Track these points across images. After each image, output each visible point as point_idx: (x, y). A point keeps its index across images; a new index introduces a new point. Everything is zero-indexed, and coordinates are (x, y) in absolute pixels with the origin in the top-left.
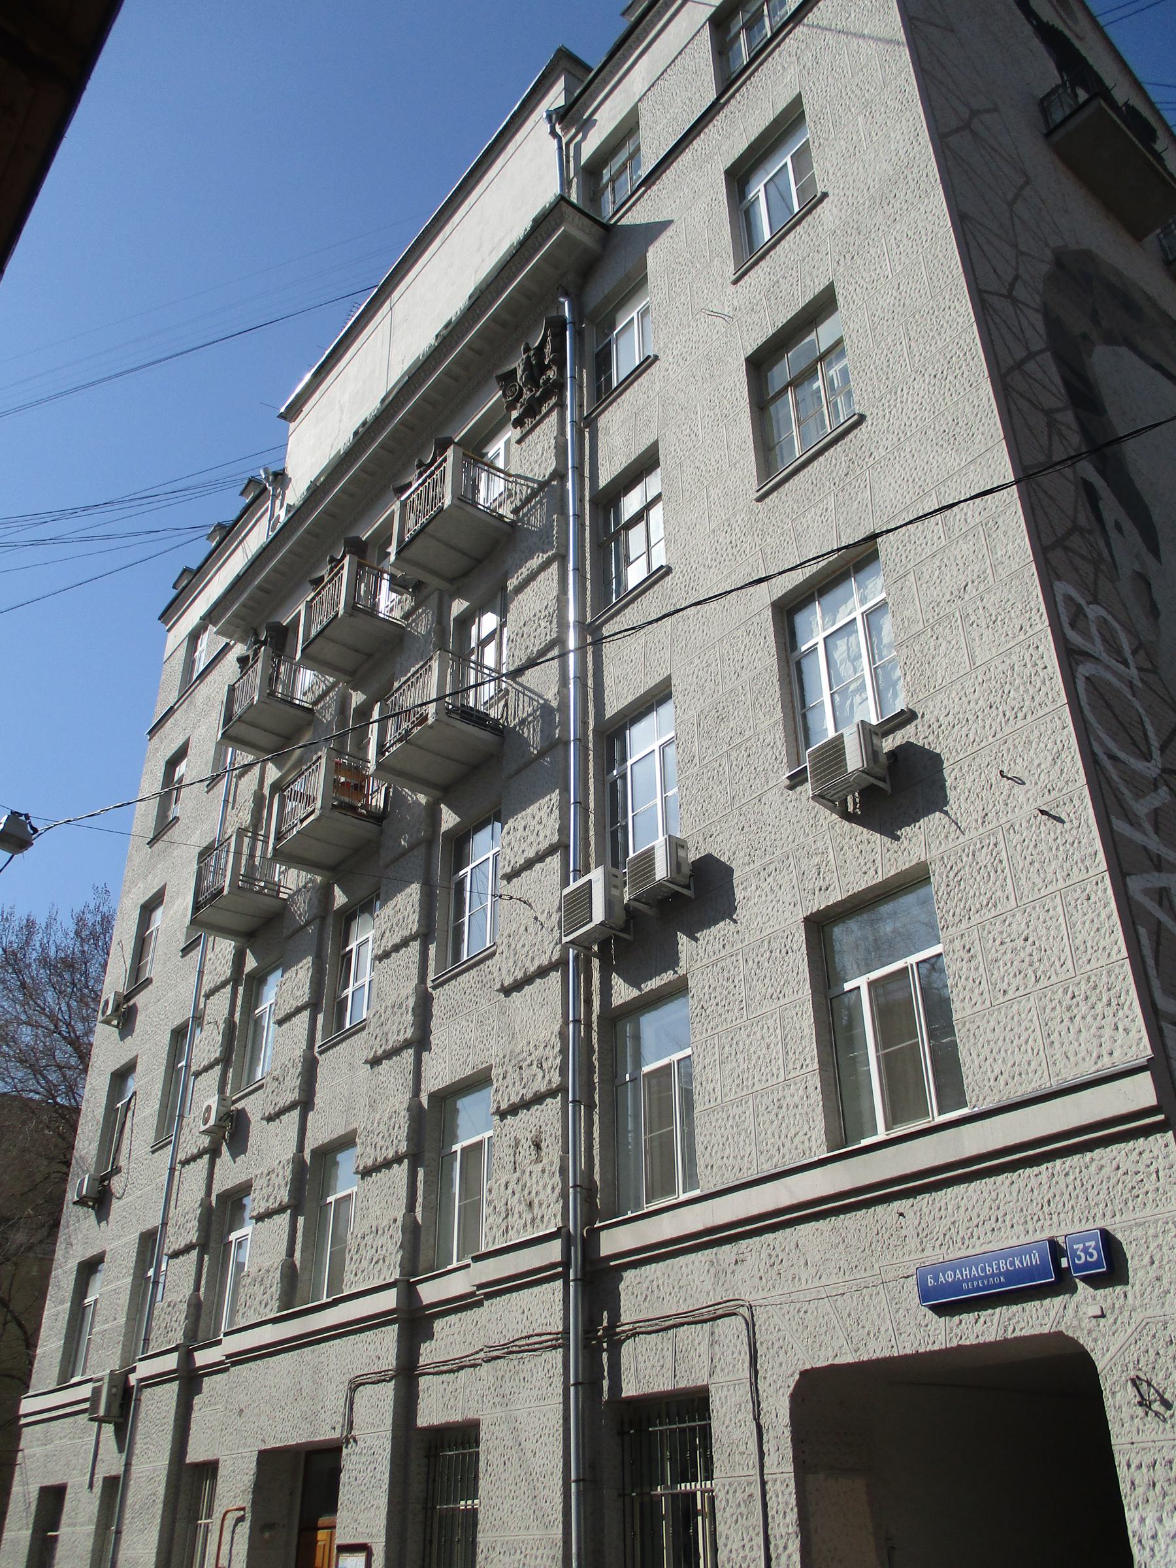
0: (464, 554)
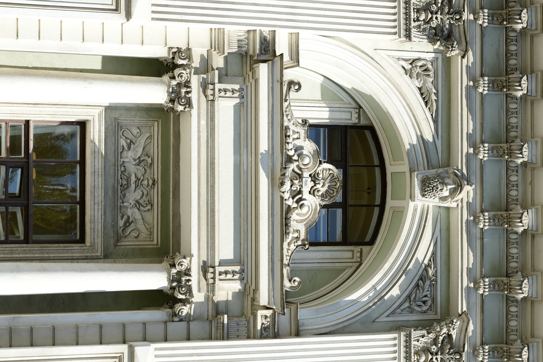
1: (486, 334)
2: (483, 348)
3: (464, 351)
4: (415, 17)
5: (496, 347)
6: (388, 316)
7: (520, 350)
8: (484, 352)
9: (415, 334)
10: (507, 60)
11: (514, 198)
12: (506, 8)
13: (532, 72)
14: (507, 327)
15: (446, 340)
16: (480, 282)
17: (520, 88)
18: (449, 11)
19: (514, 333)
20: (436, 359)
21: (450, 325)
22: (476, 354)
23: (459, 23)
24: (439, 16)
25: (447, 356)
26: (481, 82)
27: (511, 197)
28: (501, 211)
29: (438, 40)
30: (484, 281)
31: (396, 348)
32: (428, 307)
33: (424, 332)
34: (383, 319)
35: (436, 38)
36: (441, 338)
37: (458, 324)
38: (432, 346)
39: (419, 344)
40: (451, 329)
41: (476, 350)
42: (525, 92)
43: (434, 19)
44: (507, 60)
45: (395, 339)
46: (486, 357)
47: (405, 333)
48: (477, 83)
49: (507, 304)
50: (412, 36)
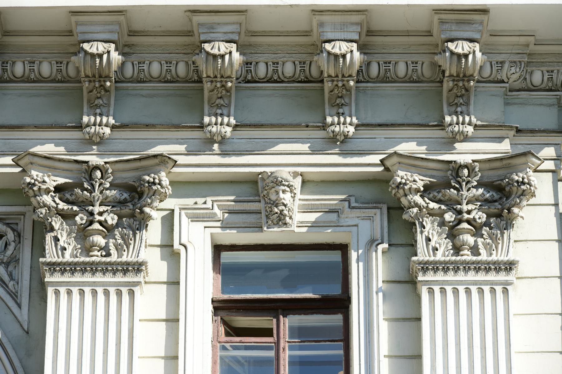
0: (399, 282)
1: (303, 118)
2: (88, 125)
3: (87, 162)
4: (99, 254)
5: (89, 101)
6: (19, 306)
7: (89, 58)
8: (94, 125)
9: (51, 255)
10: (41, 80)
11: (298, 69)
12: (80, 82)
13: (70, 33)
14: (54, 81)
15: (68, 196)
16: (333, 132)
17: (105, 57)
18: (455, 188)
19: (63, 68)
20: (101, 214)
21: (35, 188)
22: (98, 140)
23: (477, 169)
24: (97, 209)
25: (97, 193)
26: (214, 129)
27: (297, 75)
28: (441, 93)
29: (142, 212)
30: (332, 124)
31: (75, 290)
32: (9, 230)
33: (49, 237)
34: (23, 315)
35: (138, 216)
36: (62, 206)
37: (401, 175)
38: (75, 223)
39: (71, 247)
40: (44, 187)
41: (91, 138)
42: (113, 46)
43: (102, 218)
44: (41, 80)
45: (57, 293)
46: (467, 119)
47: (47, 275)
48: (215, 138)
49: (11, 81)
50: (506, 259)
